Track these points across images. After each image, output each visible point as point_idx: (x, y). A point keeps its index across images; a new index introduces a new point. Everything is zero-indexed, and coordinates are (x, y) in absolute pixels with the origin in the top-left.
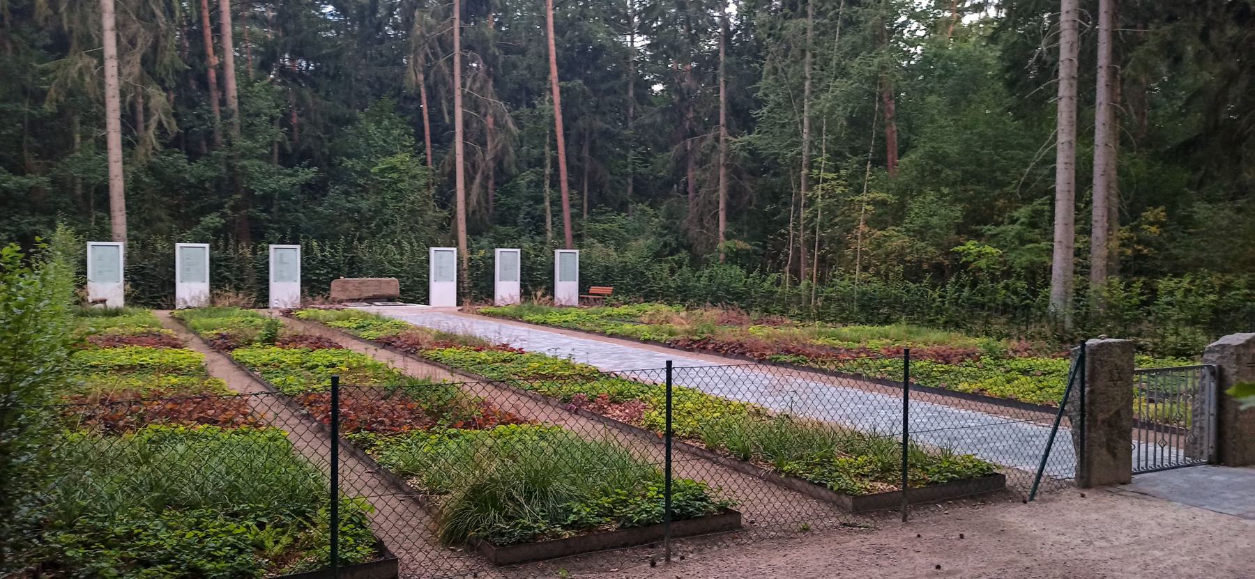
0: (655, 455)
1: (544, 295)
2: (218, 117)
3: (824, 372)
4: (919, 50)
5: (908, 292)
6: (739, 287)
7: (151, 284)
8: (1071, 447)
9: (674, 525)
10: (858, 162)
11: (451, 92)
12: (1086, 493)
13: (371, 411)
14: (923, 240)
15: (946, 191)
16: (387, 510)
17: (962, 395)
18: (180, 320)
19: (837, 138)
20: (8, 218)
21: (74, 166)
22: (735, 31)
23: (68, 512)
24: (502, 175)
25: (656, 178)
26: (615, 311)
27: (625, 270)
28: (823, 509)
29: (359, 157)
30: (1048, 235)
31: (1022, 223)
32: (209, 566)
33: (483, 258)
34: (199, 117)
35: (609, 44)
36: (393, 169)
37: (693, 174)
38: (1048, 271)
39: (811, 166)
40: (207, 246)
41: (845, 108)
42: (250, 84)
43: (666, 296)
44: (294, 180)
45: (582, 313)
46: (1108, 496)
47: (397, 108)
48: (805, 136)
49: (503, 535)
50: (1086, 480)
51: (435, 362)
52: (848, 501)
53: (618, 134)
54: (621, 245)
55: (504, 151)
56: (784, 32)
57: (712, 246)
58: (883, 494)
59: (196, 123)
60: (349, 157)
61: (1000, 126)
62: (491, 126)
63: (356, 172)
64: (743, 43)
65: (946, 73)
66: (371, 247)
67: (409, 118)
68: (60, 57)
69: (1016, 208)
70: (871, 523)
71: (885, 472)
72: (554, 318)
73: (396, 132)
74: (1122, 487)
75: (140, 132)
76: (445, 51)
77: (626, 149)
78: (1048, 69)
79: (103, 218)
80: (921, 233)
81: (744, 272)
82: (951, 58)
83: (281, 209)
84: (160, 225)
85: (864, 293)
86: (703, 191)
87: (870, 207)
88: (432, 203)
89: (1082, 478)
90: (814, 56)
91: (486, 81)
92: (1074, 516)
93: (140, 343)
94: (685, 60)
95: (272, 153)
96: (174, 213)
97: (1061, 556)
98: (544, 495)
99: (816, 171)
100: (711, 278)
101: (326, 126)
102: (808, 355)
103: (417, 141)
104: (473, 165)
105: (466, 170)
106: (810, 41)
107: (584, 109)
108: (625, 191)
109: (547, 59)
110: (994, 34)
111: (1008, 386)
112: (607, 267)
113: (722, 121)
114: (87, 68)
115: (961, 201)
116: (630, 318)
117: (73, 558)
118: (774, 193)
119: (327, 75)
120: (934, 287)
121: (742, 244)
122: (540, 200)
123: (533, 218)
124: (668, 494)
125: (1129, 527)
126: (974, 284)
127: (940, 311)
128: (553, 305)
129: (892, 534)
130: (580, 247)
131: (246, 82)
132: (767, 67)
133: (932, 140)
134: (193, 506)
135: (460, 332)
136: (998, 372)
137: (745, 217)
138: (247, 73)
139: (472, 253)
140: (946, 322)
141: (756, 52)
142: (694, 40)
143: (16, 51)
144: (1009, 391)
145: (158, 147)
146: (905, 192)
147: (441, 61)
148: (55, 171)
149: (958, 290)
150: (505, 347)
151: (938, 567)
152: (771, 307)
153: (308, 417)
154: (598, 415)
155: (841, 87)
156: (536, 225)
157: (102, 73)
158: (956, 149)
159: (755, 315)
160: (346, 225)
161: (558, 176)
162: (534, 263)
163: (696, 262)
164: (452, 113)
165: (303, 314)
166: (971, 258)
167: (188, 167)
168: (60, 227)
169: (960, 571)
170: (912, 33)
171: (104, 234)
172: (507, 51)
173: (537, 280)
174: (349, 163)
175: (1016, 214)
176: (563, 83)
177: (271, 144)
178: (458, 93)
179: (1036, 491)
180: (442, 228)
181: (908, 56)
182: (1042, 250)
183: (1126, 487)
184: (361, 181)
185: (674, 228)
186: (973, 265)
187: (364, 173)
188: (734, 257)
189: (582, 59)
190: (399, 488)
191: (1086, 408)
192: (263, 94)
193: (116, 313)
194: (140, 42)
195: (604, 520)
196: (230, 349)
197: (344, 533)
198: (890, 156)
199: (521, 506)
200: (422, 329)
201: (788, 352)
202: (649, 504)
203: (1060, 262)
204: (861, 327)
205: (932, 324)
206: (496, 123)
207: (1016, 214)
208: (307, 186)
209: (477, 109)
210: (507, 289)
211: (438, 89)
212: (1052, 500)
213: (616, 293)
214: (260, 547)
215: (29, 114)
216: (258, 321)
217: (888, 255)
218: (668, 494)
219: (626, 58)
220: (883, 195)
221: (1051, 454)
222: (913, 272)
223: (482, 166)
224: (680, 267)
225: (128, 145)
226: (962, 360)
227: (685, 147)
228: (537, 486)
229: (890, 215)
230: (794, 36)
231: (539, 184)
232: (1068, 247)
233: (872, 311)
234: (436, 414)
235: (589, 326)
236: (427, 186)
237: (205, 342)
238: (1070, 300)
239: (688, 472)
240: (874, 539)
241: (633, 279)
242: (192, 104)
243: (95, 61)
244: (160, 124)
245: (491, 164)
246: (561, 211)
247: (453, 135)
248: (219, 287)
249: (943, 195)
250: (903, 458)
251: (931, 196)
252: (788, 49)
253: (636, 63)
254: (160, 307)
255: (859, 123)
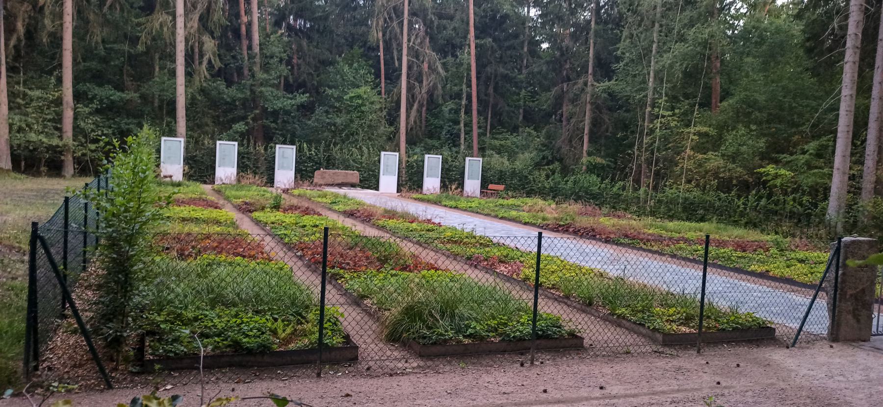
0: (527, 297)
1: (456, 189)
2: (246, 58)
3: (650, 251)
4: (742, 23)
5: (720, 199)
6: (595, 189)
7: (200, 167)
8: (827, 314)
9: (538, 342)
10: (689, 104)
11: (400, 45)
13: (342, 256)
14: (734, 162)
15: (753, 127)
16: (350, 319)
17: (753, 274)
18: (218, 192)
19: (675, 86)
20: (113, 119)
21: (153, 88)
22: (604, 6)
23: (159, 303)
24: (432, 104)
25: (540, 110)
26: (505, 202)
27: (514, 174)
28: (640, 340)
29: (336, 87)
30: (830, 163)
31: (811, 154)
32: (244, 340)
33: (416, 161)
34: (234, 57)
35: (511, 13)
36: (359, 97)
37: (567, 109)
38: (827, 190)
39: (653, 106)
40: (236, 143)
41: (681, 65)
42: (268, 36)
43: (543, 193)
44: (293, 102)
45: (483, 202)
46: (851, 348)
47: (363, 55)
48: (650, 84)
49: (425, 338)
50: (835, 336)
51: (382, 228)
52: (659, 337)
53: (515, 78)
54: (512, 156)
55: (435, 87)
56: (639, 8)
57: (577, 160)
58: (685, 334)
59: (232, 61)
60: (330, 87)
61: (800, 81)
62: (427, 70)
63: (335, 98)
64: (609, 15)
65: (759, 42)
66: (341, 149)
67: (371, 62)
68: (148, 15)
69: (807, 143)
70: (674, 352)
71: (687, 320)
72: (463, 204)
73: (362, 72)
74: (863, 343)
75: (196, 65)
76: (398, 17)
77: (521, 89)
78: (840, 40)
79: (171, 122)
80: (733, 158)
81: (599, 179)
82: (766, 30)
83: (284, 121)
84: (207, 128)
85: (686, 199)
86: (573, 120)
87: (696, 137)
88: (383, 121)
89: (832, 334)
90: (661, 26)
91: (424, 38)
92: (822, 359)
93: (195, 204)
94: (566, 26)
95: (280, 83)
96: (216, 121)
97: (808, 384)
98: (452, 316)
99: (657, 110)
100: (575, 182)
101: (316, 66)
102: (642, 240)
103: (376, 79)
104: (413, 96)
105: (407, 99)
106: (658, 15)
107: (492, 60)
108: (518, 118)
109: (468, 24)
110: (799, 13)
111: (787, 270)
112: (501, 171)
113: (590, 71)
114: (166, 22)
115: (765, 135)
116: (517, 207)
117: (165, 329)
118: (625, 124)
119: (318, 31)
120: (739, 197)
121: (599, 160)
122: (457, 123)
123: (451, 135)
124: (534, 321)
125: (863, 370)
126: (769, 196)
127: (742, 215)
128: (462, 195)
129: (688, 361)
130: (483, 156)
131: (265, 36)
132: (625, 33)
133: (746, 90)
134: (235, 305)
135: (399, 210)
136: (781, 259)
137: (603, 141)
138: (265, 29)
139: (409, 157)
140: (747, 223)
141: (619, 22)
142: (573, 12)
143: (122, 10)
144: (787, 273)
145: (208, 77)
146: (723, 128)
147: (395, 24)
148: (143, 90)
149: (757, 200)
150: (429, 221)
151: (719, 383)
152: (617, 204)
153: (300, 258)
154: (490, 269)
155: (679, 48)
156: (454, 140)
157: (174, 26)
158: (763, 98)
159: (605, 210)
160: (326, 134)
161: (471, 106)
162: (451, 166)
163: (566, 171)
164: (400, 60)
165: (296, 192)
166: (770, 178)
167: (226, 90)
168: (146, 127)
169: (733, 387)
170: (737, 10)
171: (172, 133)
172: (440, 17)
173: (452, 178)
174: (330, 92)
175: (806, 147)
176: (478, 41)
177: (280, 77)
178: (405, 46)
179: (796, 341)
180: (389, 139)
181: (732, 27)
182: (824, 174)
183: (866, 343)
184: (337, 104)
185: (551, 146)
186: (771, 182)
187: (339, 99)
188: (592, 169)
189: (492, 24)
190: (358, 305)
191: (839, 285)
192: (276, 43)
193: (179, 185)
194: (199, 6)
195: (491, 334)
196: (251, 211)
197: (326, 328)
198: (714, 101)
199: (437, 320)
200: (374, 206)
201: (626, 236)
202: (522, 326)
203: (837, 184)
204: (682, 223)
205: (736, 223)
206: (429, 67)
207: (806, 147)
208: (302, 107)
209: (417, 57)
210: (432, 183)
211: (391, 43)
212: (808, 348)
213: (506, 189)
214: (274, 332)
215: (129, 51)
216: (268, 195)
217: (707, 172)
218: (534, 321)
219: (524, 24)
220: (705, 129)
221: (809, 316)
222: (725, 186)
223: (419, 97)
224: (553, 174)
225: (189, 74)
226: (755, 250)
227: (562, 89)
228: (448, 309)
229: (707, 144)
230: (647, 11)
231: (457, 112)
232: (844, 173)
233: (691, 211)
234: (383, 261)
235: (486, 211)
236: (381, 109)
237: (235, 207)
238: (842, 211)
239: (548, 309)
240: (675, 362)
241: (520, 181)
242: (230, 49)
243: (170, 18)
244: (210, 62)
245: (425, 96)
246: (471, 131)
247: (400, 75)
248: (243, 171)
249: (751, 130)
250: (702, 311)
251: (742, 130)
252: (642, 20)
253: (530, 28)
254: (205, 183)
255: (691, 75)
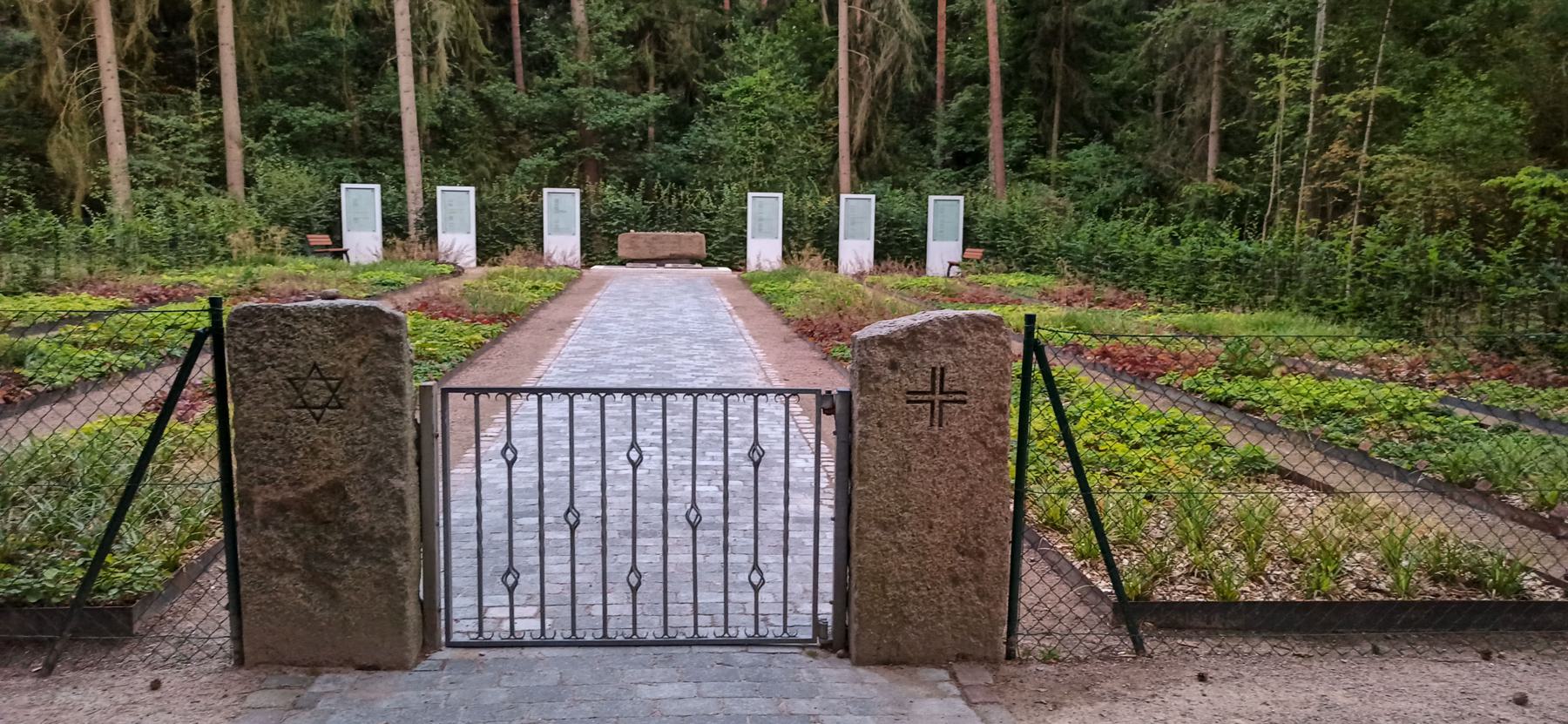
12: (1384, 647)
247: (390, 38)
